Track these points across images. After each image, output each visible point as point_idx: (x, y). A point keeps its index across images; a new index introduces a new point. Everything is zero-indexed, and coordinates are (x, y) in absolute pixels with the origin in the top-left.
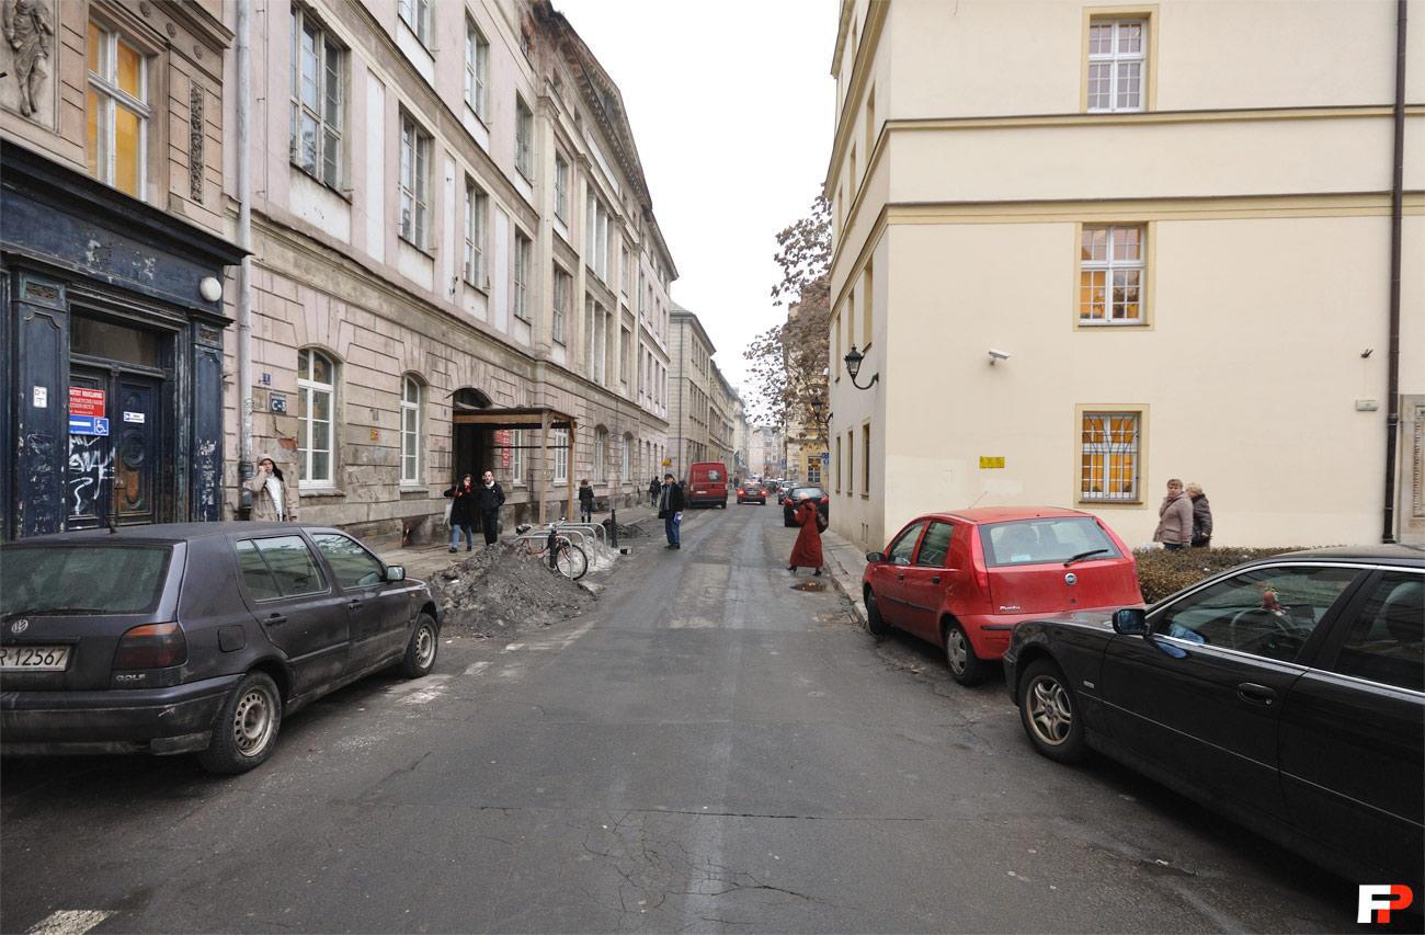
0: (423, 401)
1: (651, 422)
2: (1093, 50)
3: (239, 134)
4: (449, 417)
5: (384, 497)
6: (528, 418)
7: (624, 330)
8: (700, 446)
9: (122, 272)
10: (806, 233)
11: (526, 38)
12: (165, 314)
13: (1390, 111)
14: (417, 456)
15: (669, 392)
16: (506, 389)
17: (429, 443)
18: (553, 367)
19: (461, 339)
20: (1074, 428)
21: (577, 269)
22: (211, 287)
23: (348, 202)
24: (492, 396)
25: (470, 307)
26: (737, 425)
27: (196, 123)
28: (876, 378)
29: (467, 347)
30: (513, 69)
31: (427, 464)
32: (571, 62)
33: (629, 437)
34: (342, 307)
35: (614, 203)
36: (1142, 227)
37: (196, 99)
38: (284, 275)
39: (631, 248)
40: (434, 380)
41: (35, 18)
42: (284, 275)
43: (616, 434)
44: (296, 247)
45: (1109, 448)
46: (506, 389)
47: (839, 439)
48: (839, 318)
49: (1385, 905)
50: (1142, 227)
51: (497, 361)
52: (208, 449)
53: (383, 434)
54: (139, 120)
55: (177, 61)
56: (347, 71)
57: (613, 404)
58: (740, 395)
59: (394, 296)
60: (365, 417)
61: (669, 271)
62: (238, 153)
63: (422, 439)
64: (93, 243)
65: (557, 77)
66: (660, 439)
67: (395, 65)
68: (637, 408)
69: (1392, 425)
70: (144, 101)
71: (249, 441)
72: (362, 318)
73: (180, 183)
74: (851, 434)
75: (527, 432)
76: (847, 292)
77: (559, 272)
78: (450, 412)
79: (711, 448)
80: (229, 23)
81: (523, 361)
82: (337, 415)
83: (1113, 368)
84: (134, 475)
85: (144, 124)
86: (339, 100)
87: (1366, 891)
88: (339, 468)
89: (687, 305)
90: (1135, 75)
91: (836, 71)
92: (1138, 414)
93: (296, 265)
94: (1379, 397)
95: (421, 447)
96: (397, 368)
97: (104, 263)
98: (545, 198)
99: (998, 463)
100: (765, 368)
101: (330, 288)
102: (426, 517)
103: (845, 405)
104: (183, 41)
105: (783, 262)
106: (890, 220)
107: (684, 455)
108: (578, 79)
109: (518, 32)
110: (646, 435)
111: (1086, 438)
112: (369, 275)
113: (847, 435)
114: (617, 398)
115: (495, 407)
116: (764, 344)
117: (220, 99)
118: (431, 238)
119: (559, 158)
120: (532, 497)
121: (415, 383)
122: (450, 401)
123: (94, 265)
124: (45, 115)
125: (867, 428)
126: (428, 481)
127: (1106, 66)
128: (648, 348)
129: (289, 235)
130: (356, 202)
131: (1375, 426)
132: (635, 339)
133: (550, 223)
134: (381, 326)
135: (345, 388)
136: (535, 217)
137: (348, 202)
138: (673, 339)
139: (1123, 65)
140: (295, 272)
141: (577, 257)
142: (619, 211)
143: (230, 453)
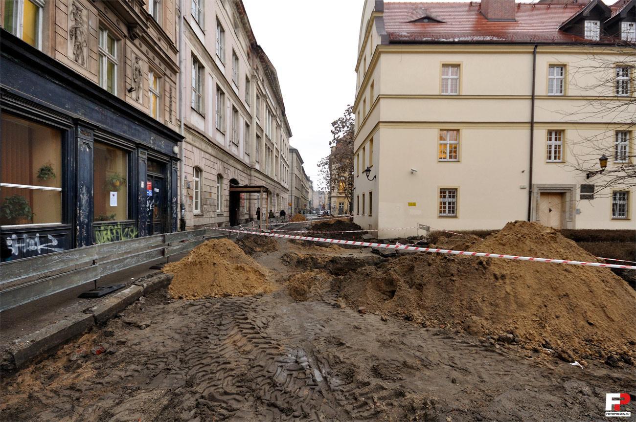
0: (221, 183)
1: (284, 190)
2: (443, 75)
3: (180, 99)
4: (229, 189)
5: (213, 216)
6: (251, 189)
7: (276, 156)
8: (299, 199)
9: (158, 146)
10: (342, 122)
11: (248, 54)
12: (165, 158)
13: (531, 97)
14: (220, 202)
15: (288, 178)
16: (243, 179)
17: (224, 197)
18: (257, 171)
19: (231, 162)
20: (437, 194)
21: (263, 135)
22: (176, 149)
23: (204, 118)
24: (239, 181)
25: (233, 151)
26: (310, 190)
27: (171, 98)
28: (375, 177)
29: (233, 165)
30: (245, 67)
31: (223, 205)
32: (262, 62)
33: (278, 195)
34: (203, 153)
35: (273, 111)
36: (458, 130)
37: (171, 90)
38: (190, 144)
39: (279, 126)
40: (225, 176)
41: (140, 72)
42: (190, 144)
43: (274, 194)
44: (192, 134)
45: (447, 200)
46: (243, 179)
47: (358, 197)
48: (358, 155)
49: (618, 402)
50: (458, 130)
51: (241, 169)
52: (174, 200)
53: (213, 194)
54: (156, 98)
55: (167, 79)
56: (204, 75)
57: (273, 183)
58: (311, 179)
59: (215, 148)
60: (208, 189)
61: (289, 134)
62: (180, 105)
63: (221, 196)
64: (152, 138)
65: (257, 68)
66: (287, 196)
67: (215, 70)
68: (280, 184)
69: (530, 193)
70: (158, 92)
71: (184, 197)
72: (207, 156)
73: (167, 118)
74: (364, 195)
75: (248, 194)
76: (362, 147)
77: (258, 137)
78: (229, 187)
79: (302, 199)
80: (178, 64)
81: (248, 168)
82: (201, 189)
83: (449, 175)
84: (157, 208)
85: (158, 99)
86: (201, 84)
87: (609, 396)
88: (202, 206)
89: (295, 147)
90: (457, 82)
91: (357, 70)
92: (456, 189)
93: (192, 140)
94: (527, 185)
95: (221, 199)
96: (216, 173)
97: (154, 144)
98: (253, 111)
99: (414, 204)
100: (324, 170)
101: (200, 147)
102: (223, 223)
103: (361, 185)
104: (168, 72)
105: (333, 133)
106: (380, 127)
107: (293, 202)
108: (264, 68)
109: (246, 53)
110: (283, 195)
111: (441, 197)
112: (210, 142)
113: (368, 194)
114: (274, 181)
115: (240, 185)
116: (324, 161)
117: (175, 89)
118: (224, 127)
119: (257, 96)
120: (250, 216)
121: (220, 177)
122: (229, 184)
123: (153, 144)
124: (141, 101)
125: (371, 193)
126: (223, 210)
127: (447, 79)
128: (283, 163)
129: (191, 131)
130: (206, 118)
131: (525, 193)
132: (280, 159)
133: (255, 120)
134: (212, 159)
135: (204, 180)
136: (251, 117)
137: (204, 118)
138: (288, 157)
139: (452, 79)
140: (192, 142)
141: (262, 131)
142: (275, 114)
143: (179, 202)
